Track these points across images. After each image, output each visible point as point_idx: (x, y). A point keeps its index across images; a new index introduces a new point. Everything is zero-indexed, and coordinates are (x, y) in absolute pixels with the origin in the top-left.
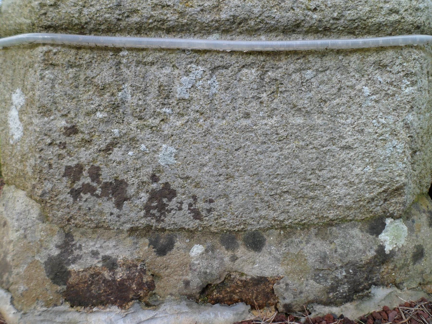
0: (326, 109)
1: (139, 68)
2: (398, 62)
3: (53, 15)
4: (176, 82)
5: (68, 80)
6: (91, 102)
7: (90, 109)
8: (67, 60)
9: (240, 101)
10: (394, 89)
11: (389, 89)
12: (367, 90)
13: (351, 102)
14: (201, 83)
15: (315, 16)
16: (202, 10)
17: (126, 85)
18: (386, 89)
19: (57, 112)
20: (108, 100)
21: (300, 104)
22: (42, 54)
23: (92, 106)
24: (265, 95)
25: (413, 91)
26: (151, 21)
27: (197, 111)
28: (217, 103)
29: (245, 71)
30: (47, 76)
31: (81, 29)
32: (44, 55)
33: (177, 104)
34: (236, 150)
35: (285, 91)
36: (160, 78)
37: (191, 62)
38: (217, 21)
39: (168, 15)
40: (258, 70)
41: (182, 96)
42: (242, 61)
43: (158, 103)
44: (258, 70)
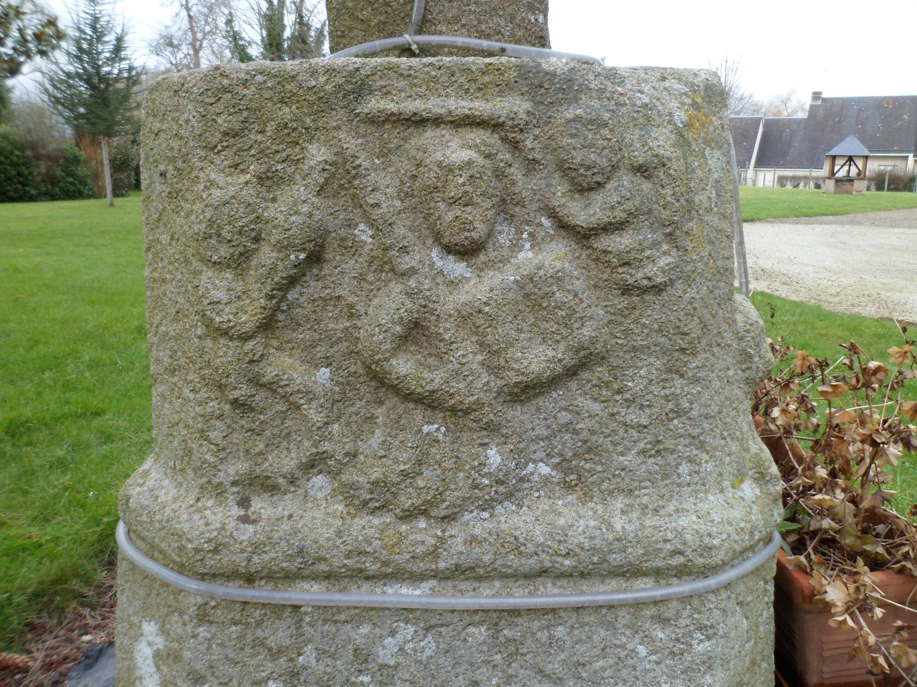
0: (585, 675)
1: (327, 627)
2: (685, 614)
3: (212, 562)
4: (378, 644)
5: (230, 641)
6: (262, 668)
7: (259, 678)
8: (229, 617)
9: (465, 666)
10: (682, 647)
11: (674, 646)
12: (642, 650)
13: (621, 665)
14: (411, 645)
15: (567, 562)
16: (413, 557)
17: (309, 647)
18: (671, 646)
19: (213, 678)
20: (284, 667)
21: (548, 669)
22: (195, 608)
23: (263, 674)
24: (499, 657)
25: (709, 649)
26: (343, 570)
27: (406, 680)
28: (433, 667)
29: (472, 629)
30: (201, 635)
31: (250, 579)
32: (199, 609)
33: (379, 670)
34: (772, 316)
35: (529, 652)
36: (355, 640)
37: (397, 621)
38: (433, 570)
39: (367, 565)
40: (489, 629)
41: (386, 661)
42: (467, 619)
43: (353, 670)
44: (489, 629)
